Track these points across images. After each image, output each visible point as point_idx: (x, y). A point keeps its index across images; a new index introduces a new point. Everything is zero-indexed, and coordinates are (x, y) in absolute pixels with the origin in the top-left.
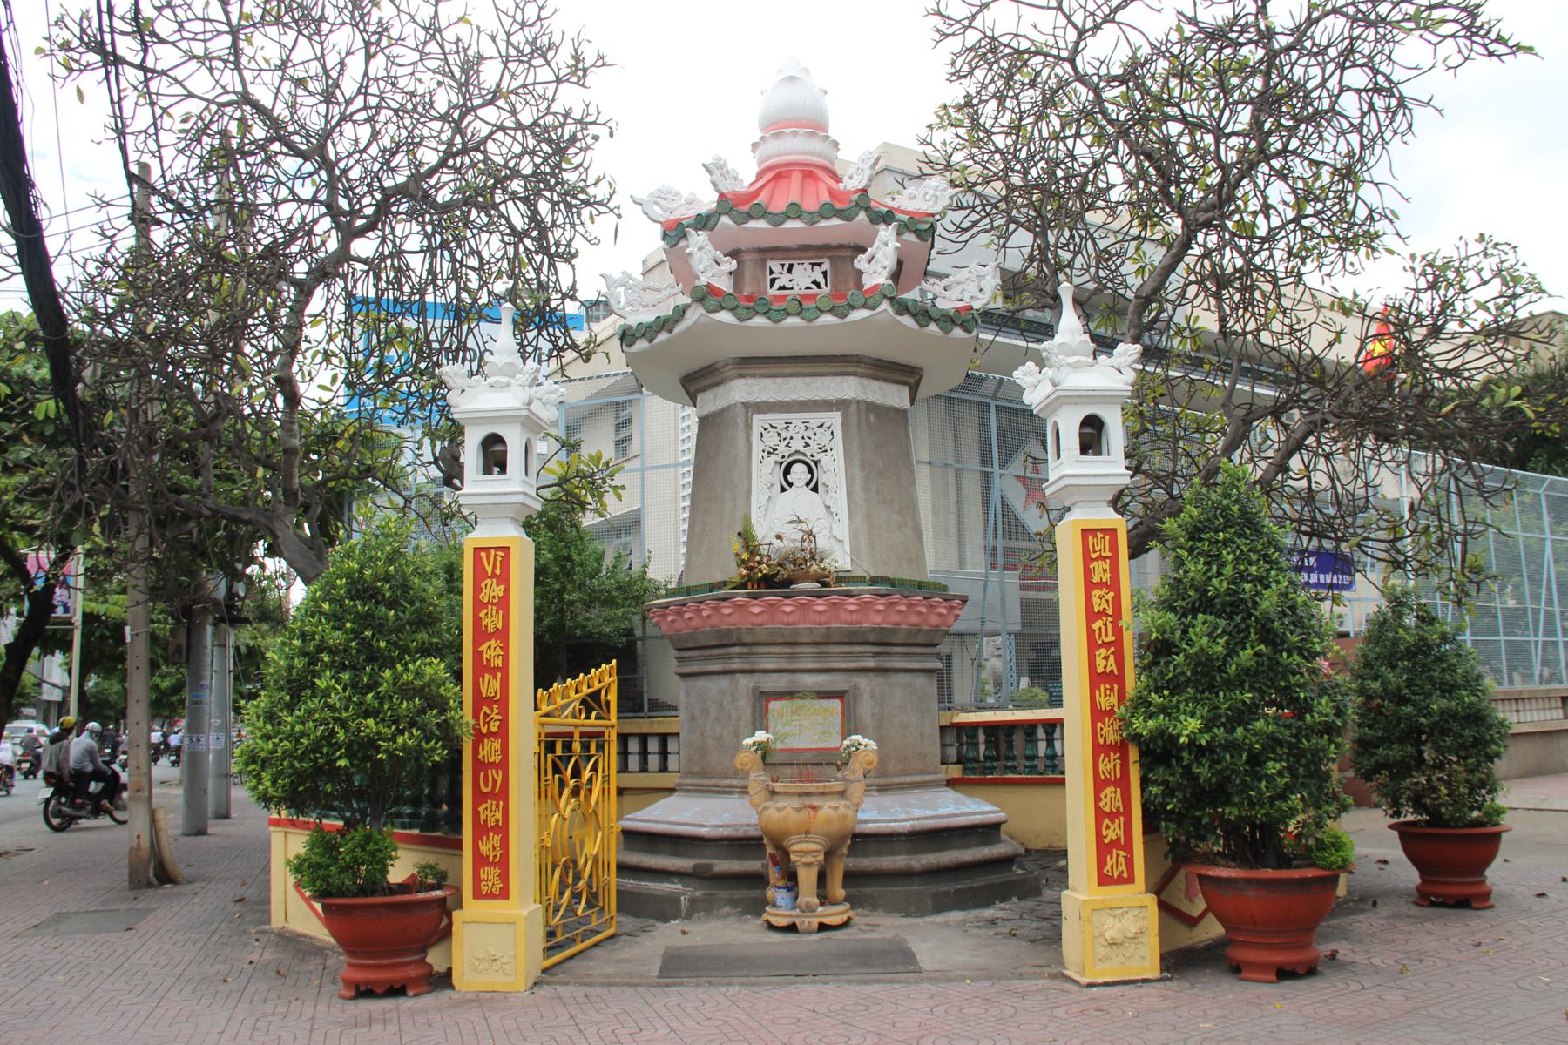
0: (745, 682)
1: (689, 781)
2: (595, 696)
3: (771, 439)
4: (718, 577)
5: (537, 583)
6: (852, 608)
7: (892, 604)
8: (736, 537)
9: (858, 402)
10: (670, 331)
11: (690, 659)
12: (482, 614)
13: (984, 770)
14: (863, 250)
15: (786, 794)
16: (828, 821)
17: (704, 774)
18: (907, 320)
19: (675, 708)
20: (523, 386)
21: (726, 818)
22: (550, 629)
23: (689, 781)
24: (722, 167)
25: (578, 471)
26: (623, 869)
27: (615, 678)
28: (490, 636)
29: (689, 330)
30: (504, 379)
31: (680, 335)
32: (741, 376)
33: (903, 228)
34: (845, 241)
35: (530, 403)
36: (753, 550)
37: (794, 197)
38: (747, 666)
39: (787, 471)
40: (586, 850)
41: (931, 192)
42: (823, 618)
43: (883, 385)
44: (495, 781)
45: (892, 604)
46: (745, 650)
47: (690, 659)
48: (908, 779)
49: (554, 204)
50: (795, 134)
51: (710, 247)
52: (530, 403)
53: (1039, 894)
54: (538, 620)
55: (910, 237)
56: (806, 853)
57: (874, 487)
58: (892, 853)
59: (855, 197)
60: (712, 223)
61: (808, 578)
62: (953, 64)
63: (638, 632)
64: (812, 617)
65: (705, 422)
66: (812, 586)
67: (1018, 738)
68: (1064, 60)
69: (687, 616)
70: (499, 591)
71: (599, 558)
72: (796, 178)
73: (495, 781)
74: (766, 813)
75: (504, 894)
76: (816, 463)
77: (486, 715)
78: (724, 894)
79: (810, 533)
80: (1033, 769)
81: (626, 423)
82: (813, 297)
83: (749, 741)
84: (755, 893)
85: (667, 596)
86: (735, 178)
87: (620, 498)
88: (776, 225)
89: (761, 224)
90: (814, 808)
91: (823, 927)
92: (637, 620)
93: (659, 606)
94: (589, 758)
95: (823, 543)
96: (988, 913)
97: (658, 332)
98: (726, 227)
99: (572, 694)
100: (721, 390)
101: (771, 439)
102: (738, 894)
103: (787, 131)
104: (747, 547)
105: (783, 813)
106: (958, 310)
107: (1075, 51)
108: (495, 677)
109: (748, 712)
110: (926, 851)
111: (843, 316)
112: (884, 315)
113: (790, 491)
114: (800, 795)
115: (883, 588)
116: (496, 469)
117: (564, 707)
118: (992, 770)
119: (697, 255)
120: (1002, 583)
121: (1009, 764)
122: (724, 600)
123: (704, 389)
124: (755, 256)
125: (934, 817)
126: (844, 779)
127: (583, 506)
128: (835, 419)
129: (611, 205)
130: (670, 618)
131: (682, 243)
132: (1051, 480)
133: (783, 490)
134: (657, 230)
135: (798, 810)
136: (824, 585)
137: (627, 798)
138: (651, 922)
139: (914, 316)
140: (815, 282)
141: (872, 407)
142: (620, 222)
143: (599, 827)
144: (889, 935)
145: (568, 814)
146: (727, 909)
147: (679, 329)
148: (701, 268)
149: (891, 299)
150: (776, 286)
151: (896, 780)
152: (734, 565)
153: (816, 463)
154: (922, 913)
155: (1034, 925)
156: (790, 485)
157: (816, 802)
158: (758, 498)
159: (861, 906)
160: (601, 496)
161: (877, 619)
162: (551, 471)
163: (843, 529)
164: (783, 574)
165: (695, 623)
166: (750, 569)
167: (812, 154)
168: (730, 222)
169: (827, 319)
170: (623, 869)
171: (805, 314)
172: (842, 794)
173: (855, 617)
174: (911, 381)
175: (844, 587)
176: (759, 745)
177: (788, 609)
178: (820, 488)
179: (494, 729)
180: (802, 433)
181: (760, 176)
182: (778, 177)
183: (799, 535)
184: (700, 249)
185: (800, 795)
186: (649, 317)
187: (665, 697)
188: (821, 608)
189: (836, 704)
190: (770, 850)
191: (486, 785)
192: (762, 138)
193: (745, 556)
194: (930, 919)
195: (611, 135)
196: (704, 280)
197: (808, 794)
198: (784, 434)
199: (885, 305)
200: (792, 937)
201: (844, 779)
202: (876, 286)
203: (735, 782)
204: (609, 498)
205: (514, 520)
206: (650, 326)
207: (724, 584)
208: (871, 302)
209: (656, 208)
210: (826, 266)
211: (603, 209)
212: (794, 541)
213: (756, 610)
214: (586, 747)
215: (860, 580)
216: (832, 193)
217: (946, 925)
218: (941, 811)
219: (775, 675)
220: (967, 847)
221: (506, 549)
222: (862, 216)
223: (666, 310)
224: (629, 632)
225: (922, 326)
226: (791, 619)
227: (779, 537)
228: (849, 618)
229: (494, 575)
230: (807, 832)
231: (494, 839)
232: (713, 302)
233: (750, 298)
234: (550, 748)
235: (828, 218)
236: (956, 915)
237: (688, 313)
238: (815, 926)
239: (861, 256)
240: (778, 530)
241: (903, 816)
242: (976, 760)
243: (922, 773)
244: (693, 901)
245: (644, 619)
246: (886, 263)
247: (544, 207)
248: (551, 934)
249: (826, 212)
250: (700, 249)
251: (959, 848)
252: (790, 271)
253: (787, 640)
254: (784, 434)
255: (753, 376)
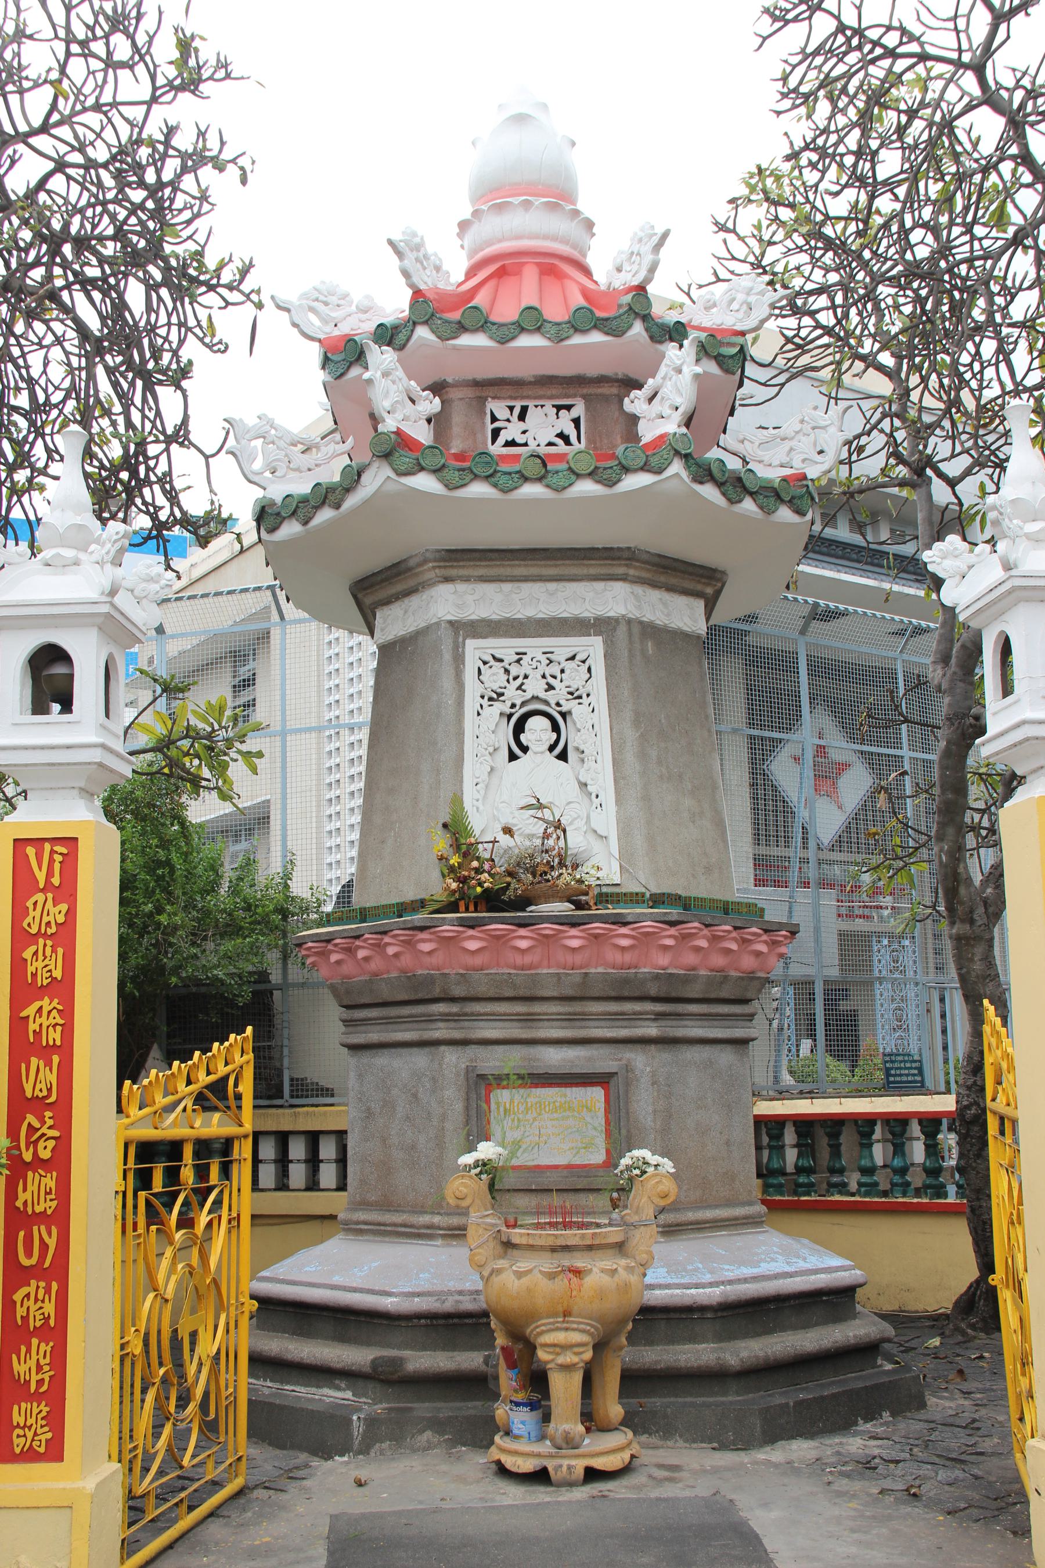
0: (453, 1059)
1: (362, 1216)
2: (219, 1087)
3: (495, 678)
4: (410, 894)
5: (123, 902)
6: (625, 942)
7: (686, 937)
8: (440, 831)
9: (629, 622)
10: (338, 506)
11: (364, 1021)
12: (28, 954)
13: (797, 1189)
14: (635, 384)
15: (531, 1247)
16: (601, 1294)
17: (386, 1205)
18: (709, 492)
19: (329, 1092)
20: (100, 563)
21: (424, 1281)
22: (143, 969)
23: (362, 1216)
24: (417, 248)
25: (188, 728)
26: (260, 1363)
27: (250, 1056)
28: (43, 991)
29: (366, 502)
30: (69, 553)
31: (356, 511)
32: (447, 580)
33: (704, 351)
34: (608, 371)
35: (113, 593)
36: (468, 853)
37: (530, 299)
38: (457, 1035)
39: (519, 729)
40: (199, 1350)
41: (741, 297)
42: (578, 959)
43: (667, 596)
44: (44, 1246)
45: (686, 937)
46: (454, 1008)
47: (364, 1021)
48: (709, 1214)
49: (151, 287)
50: (527, 205)
51: (400, 373)
52: (113, 593)
53: (922, 1405)
54: (123, 957)
55: (711, 367)
56: (565, 1347)
57: (654, 753)
58: (693, 1339)
59: (627, 299)
60: (401, 337)
61: (555, 895)
62: (785, 79)
63: (275, 977)
64: (561, 956)
65: (386, 652)
66: (562, 908)
67: (848, 1139)
68: (966, 67)
69: (361, 954)
70: (58, 913)
71: (214, 867)
72: (530, 275)
73: (44, 1246)
74: (496, 1280)
75: (55, 1452)
76: (564, 715)
77: (31, 1129)
78: (423, 1409)
79: (558, 825)
80: (871, 1188)
81: (248, 683)
82: (561, 457)
83: (468, 1159)
84: (472, 1408)
85: (320, 924)
86: (438, 269)
87: (254, 771)
88: (503, 341)
89: (479, 340)
90: (577, 1272)
91: (592, 1475)
92: (273, 957)
93: (317, 939)
94: (210, 1189)
95: (576, 841)
96: (855, 1444)
97: (317, 508)
98: (424, 344)
99: (182, 1087)
100: (414, 602)
101: (495, 678)
102: (447, 1408)
103: (516, 200)
104: (456, 846)
105: (525, 1280)
106: (784, 479)
107: (988, 50)
108: (49, 1064)
109: (459, 1106)
110: (746, 1335)
111: (611, 483)
112: (675, 482)
113: (525, 759)
114: (553, 1249)
115: (674, 912)
116: (56, 707)
117: (170, 1108)
118: (809, 1188)
119: (381, 385)
120: (816, 906)
121: (835, 1179)
122: (422, 929)
123: (387, 602)
124: (469, 392)
125: (755, 1279)
126: (624, 1223)
127: (196, 783)
128: (594, 647)
129: (246, 287)
130: (334, 958)
131: (355, 372)
132: (992, 730)
133: (513, 757)
134: (314, 352)
135: (551, 1276)
136: (579, 906)
137: (258, 1221)
138: (303, 1457)
139: (720, 485)
140: (561, 435)
141: (649, 631)
142: (261, 315)
143: (220, 1306)
144: (703, 1489)
145: (170, 1292)
146: (428, 1435)
147: (351, 501)
148: (387, 404)
149: (687, 457)
150: (501, 440)
151: (690, 1216)
152: (436, 874)
153: (564, 715)
154: (745, 1444)
155: (942, 1475)
156: (525, 749)
157: (580, 1261)
158: (473, 770)
159: (646, 1431)
160: (225, 766)
161: (663, 960)
162: (146, 729)
163: (607, 820)
164: (517, 889)
165: (373, 966)
166: (463, 880)
167: (555, 238)
168: (432, 337)
169: (587, 487)
170: (260, 1363)
171: (551, 479)
172: (620, 1247)
173: (628, 957)
174: (709, 590)
175: (611, 910)
176: (483, 1165)
177: (523, 944)
178: (571, 754)
179: (45, 1154)
180: (543, 668)
181: (470, 274)
182: (502, 273)
183: (539, 828)
184: (386, 374)
185: (553, 1249)
186: (303, 488)
187: (315, 1073)
188: (575, 943)
189: (596, 1094)
190: (500, 1341)
191: (29, 1254)
192: (476, 213)
193: (455, 860)
194: (762, 1455)
195: (244, 181)
196: (389, 425)
197: (566, 1248)
198: (514, 670)
199: (677, 467)
200: (541, 1494)
201: (624, 1223)
202: (662, 437)
203: (436, 1219)
204: (237, 770)
205: (87, 793)
206: (304, 500)
207: (422, 904)
208: (654, 461)
209: (312, 317)
210: (579, 410)
211: (234, 297)
212: (530, 837)
213: (473, 945)
214: (202, 1173)
215: (636, 898)
216: (586, 293)
217: (790, 1468)
218: (765, 1268)
219: (500, 1049)
220: (806, 1326)
221: (72, 842)
222: (638, 328)
223: (332, 474)
224: (263, 976)
225: (731, 501)
226: (528, 959)
227: (508, 831)
228: (618, 958)
229: (48, 887)
230: (566, 1314)
231: (40, 1350)
232: (406, 459)
233: (460, 457)
234: (144, 1180)
235: (584, 332)
236: (801, 1449)
237: (365, 478)
238: (580, 1472)
239: (635, 393)
240: (507, 820)
241: (708, 1278)
242: (783, 1173)
243: (729, 1203)
244: (371, 1422)
245: (285, 957)
246: (678, 401)
247: (135, 294)
248: (134, 1506)
249: (578, 324)
250: (386, 374)
251: (795, 1328)
252: (522, 417)
253: (522, 993)
254: (514, 670)
255: (467, 579)
